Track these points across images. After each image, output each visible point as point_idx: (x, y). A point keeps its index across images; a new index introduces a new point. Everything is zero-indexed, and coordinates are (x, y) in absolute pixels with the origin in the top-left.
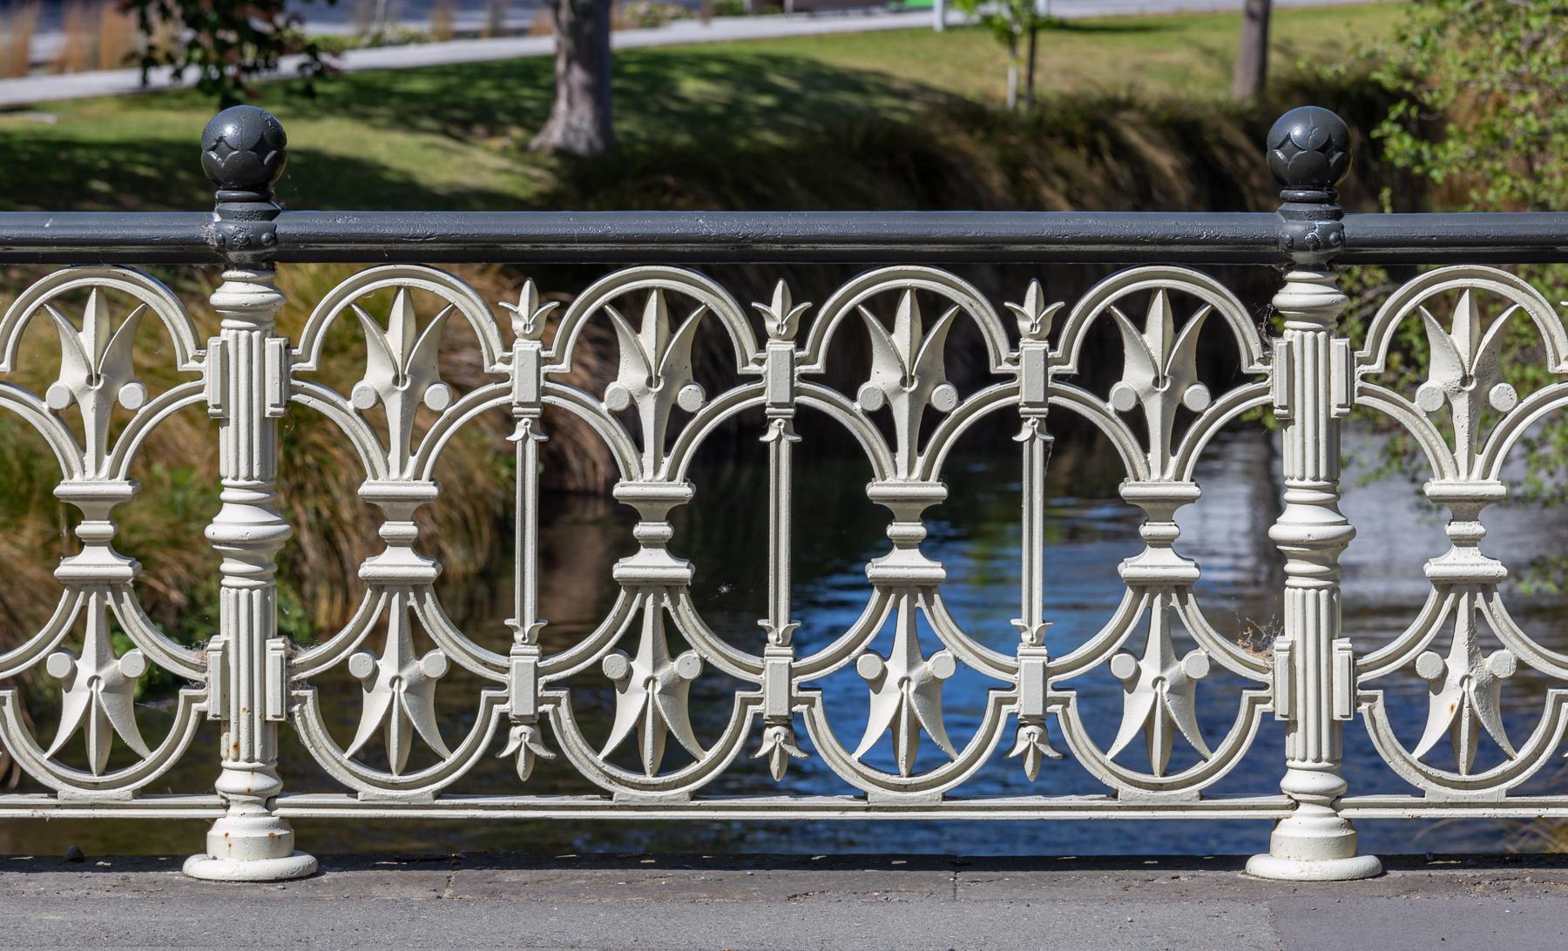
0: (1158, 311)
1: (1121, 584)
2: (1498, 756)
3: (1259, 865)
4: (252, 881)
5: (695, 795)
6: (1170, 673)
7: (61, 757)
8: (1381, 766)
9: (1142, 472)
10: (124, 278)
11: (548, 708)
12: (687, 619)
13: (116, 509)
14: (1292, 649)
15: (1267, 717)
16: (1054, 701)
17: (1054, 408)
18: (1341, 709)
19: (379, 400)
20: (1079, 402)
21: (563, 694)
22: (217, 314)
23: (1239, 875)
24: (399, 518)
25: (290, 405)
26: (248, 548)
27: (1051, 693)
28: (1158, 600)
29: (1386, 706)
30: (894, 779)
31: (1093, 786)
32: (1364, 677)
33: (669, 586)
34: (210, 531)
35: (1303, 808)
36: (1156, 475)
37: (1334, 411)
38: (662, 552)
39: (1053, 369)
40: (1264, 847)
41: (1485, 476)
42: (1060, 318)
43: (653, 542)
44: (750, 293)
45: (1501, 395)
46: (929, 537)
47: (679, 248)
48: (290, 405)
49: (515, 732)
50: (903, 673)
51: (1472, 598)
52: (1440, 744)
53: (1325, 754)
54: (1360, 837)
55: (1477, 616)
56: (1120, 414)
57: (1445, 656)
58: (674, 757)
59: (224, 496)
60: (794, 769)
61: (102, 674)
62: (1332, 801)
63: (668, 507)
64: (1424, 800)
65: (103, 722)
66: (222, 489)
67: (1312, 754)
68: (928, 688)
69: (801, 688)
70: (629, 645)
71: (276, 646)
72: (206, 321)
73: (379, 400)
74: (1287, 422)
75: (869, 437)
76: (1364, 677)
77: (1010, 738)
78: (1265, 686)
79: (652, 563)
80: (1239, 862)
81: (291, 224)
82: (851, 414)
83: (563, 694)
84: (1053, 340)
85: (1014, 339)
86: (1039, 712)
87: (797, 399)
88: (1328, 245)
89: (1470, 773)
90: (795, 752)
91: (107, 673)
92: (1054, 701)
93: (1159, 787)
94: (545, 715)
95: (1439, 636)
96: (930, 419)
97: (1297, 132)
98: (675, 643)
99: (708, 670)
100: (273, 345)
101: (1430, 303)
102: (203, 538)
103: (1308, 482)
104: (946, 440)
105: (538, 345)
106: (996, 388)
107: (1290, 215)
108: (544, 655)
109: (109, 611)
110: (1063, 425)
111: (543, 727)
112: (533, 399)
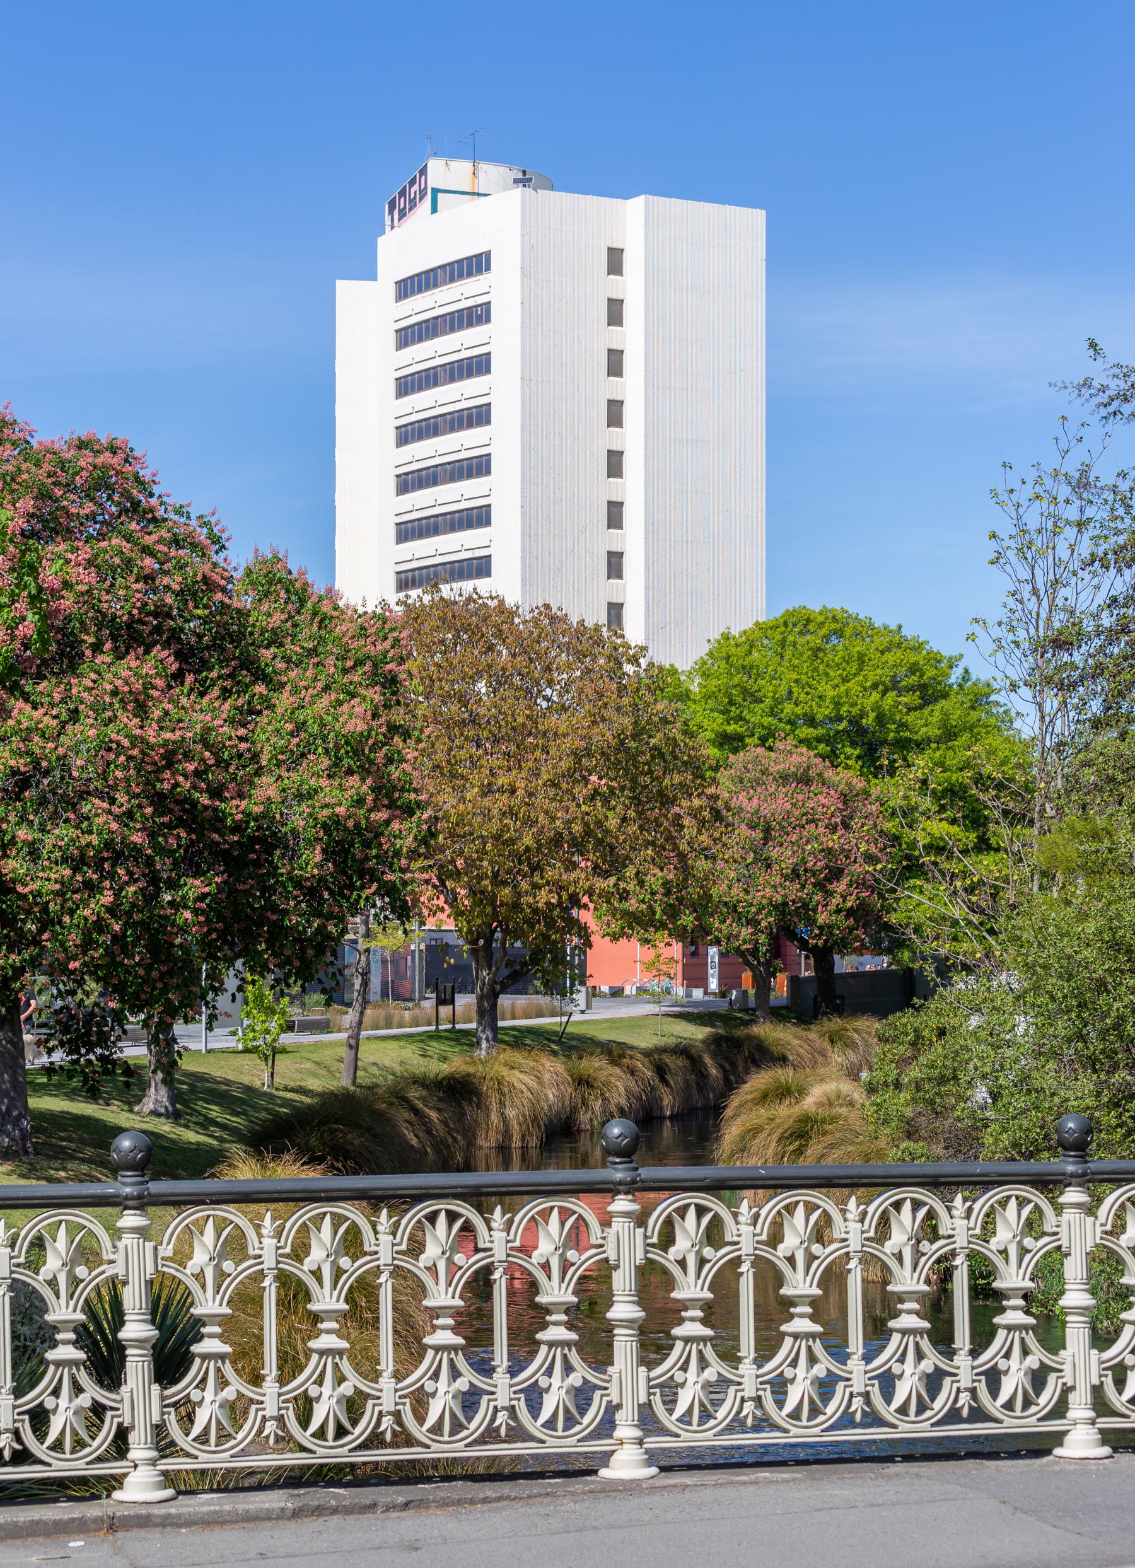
0: (801, 1208)
1: (783, 1335)
2: (229, 1437)
3: (604, 1473)
4: (160, 1502)
5: (932, 1425)
6: (336, 1393)
7: (53, 1448)
8: (658, 1421)
9: (204, 1303)
10: (458, 1205)
11: (283, 1412)
12: (84, 1378)
13: (222, 1320)
14: (131, 1392)
15: (120, 1425)
16: (19, 1421)
17: (14, 1280)
18: (643, 1399)
19: (202, 1270)
20: (406, 1263)
21: (522, 1396)
22: (611, 1215)
23: (1051, 1458)
24: (803, 1305)
25: (647, 1259)
26: (629, 1323)
27: (16, 1417)
28: (66, 1370)
29: (881, 1389)
30: (690, 1428)
31: (531, 1438)
32: (652, 1383)
33: (75, 1363)
34: (609, 1315)
35: (625, 1446)
36: (801, 1285)
37: (148, 1277)
38: (563, 1328)
39: (510, 1245)
40: (1061, 1444)
41: (338, 1301)
42: (398, 1223)
43: (66, 1342)
44: (483, 1209)
45: (228, 1266)
46: (705, 1317)
47: (844, 1181)
48: (647, 1259)
49: (385, 1419)
50: (66, 1405)
51: (334, 1358)
52: (57, 1440)
53: (149, 1440)
54: (652, 1457)
55: (336, 1366)
56: (193, 1275)
57: (437, 1382)
58: (79, 1444)
59: (615, 1299)
60: (278, 1439)
61: (450, 1389)
62: (153, 1462)
63: (73, 1325)
64: (52, 1468)
65: (74, 1433)
66: (614, 1295)
67: (143, 1441)
68: (707, 1385)
69: (400, 1397)
70: (56, 1393)
71: (156, 1388)
72: (116, 1234)
73: (202, 1270)
74: (617, 1267)
75: (47, 1293)
76: (652, 1383)
77: (379, 1423)
78: (118, 1409)
79: (557, 1333)
80: (595, 1472)
81: (156, 1187)
82: (303, 1271)
83: (983, 1378)
84: (394, 1234)
85: (260, 1236)
86: (276, 1414)
87: (510, 1259)
88: (144, 1197)
89: (563, 1431)
90: (280, 1433)
91: (74, 1405)
92: (19, 1421)
93: (214, 1452)
94: (399, 1411)
95: (200, 1383)
96: (338, 1273)
97: (1071, 1125)
98: (78, 1389)
99: (585, 1381)
100: (150, 1245)
101: (676, 1210)
102: (605, 1318)
103: (136, 1311)
104: (230, 1288)
105: (275, 1241)
106: (368, 1258)
107: (124, 1184)
108: (280, 1388)
109: (452, 1360)
110: (283, 1279)
111: (397, 1415)
112: (274, 1266)
